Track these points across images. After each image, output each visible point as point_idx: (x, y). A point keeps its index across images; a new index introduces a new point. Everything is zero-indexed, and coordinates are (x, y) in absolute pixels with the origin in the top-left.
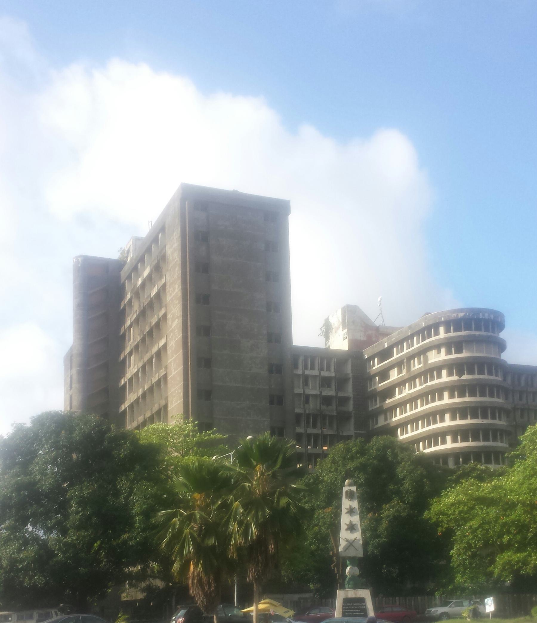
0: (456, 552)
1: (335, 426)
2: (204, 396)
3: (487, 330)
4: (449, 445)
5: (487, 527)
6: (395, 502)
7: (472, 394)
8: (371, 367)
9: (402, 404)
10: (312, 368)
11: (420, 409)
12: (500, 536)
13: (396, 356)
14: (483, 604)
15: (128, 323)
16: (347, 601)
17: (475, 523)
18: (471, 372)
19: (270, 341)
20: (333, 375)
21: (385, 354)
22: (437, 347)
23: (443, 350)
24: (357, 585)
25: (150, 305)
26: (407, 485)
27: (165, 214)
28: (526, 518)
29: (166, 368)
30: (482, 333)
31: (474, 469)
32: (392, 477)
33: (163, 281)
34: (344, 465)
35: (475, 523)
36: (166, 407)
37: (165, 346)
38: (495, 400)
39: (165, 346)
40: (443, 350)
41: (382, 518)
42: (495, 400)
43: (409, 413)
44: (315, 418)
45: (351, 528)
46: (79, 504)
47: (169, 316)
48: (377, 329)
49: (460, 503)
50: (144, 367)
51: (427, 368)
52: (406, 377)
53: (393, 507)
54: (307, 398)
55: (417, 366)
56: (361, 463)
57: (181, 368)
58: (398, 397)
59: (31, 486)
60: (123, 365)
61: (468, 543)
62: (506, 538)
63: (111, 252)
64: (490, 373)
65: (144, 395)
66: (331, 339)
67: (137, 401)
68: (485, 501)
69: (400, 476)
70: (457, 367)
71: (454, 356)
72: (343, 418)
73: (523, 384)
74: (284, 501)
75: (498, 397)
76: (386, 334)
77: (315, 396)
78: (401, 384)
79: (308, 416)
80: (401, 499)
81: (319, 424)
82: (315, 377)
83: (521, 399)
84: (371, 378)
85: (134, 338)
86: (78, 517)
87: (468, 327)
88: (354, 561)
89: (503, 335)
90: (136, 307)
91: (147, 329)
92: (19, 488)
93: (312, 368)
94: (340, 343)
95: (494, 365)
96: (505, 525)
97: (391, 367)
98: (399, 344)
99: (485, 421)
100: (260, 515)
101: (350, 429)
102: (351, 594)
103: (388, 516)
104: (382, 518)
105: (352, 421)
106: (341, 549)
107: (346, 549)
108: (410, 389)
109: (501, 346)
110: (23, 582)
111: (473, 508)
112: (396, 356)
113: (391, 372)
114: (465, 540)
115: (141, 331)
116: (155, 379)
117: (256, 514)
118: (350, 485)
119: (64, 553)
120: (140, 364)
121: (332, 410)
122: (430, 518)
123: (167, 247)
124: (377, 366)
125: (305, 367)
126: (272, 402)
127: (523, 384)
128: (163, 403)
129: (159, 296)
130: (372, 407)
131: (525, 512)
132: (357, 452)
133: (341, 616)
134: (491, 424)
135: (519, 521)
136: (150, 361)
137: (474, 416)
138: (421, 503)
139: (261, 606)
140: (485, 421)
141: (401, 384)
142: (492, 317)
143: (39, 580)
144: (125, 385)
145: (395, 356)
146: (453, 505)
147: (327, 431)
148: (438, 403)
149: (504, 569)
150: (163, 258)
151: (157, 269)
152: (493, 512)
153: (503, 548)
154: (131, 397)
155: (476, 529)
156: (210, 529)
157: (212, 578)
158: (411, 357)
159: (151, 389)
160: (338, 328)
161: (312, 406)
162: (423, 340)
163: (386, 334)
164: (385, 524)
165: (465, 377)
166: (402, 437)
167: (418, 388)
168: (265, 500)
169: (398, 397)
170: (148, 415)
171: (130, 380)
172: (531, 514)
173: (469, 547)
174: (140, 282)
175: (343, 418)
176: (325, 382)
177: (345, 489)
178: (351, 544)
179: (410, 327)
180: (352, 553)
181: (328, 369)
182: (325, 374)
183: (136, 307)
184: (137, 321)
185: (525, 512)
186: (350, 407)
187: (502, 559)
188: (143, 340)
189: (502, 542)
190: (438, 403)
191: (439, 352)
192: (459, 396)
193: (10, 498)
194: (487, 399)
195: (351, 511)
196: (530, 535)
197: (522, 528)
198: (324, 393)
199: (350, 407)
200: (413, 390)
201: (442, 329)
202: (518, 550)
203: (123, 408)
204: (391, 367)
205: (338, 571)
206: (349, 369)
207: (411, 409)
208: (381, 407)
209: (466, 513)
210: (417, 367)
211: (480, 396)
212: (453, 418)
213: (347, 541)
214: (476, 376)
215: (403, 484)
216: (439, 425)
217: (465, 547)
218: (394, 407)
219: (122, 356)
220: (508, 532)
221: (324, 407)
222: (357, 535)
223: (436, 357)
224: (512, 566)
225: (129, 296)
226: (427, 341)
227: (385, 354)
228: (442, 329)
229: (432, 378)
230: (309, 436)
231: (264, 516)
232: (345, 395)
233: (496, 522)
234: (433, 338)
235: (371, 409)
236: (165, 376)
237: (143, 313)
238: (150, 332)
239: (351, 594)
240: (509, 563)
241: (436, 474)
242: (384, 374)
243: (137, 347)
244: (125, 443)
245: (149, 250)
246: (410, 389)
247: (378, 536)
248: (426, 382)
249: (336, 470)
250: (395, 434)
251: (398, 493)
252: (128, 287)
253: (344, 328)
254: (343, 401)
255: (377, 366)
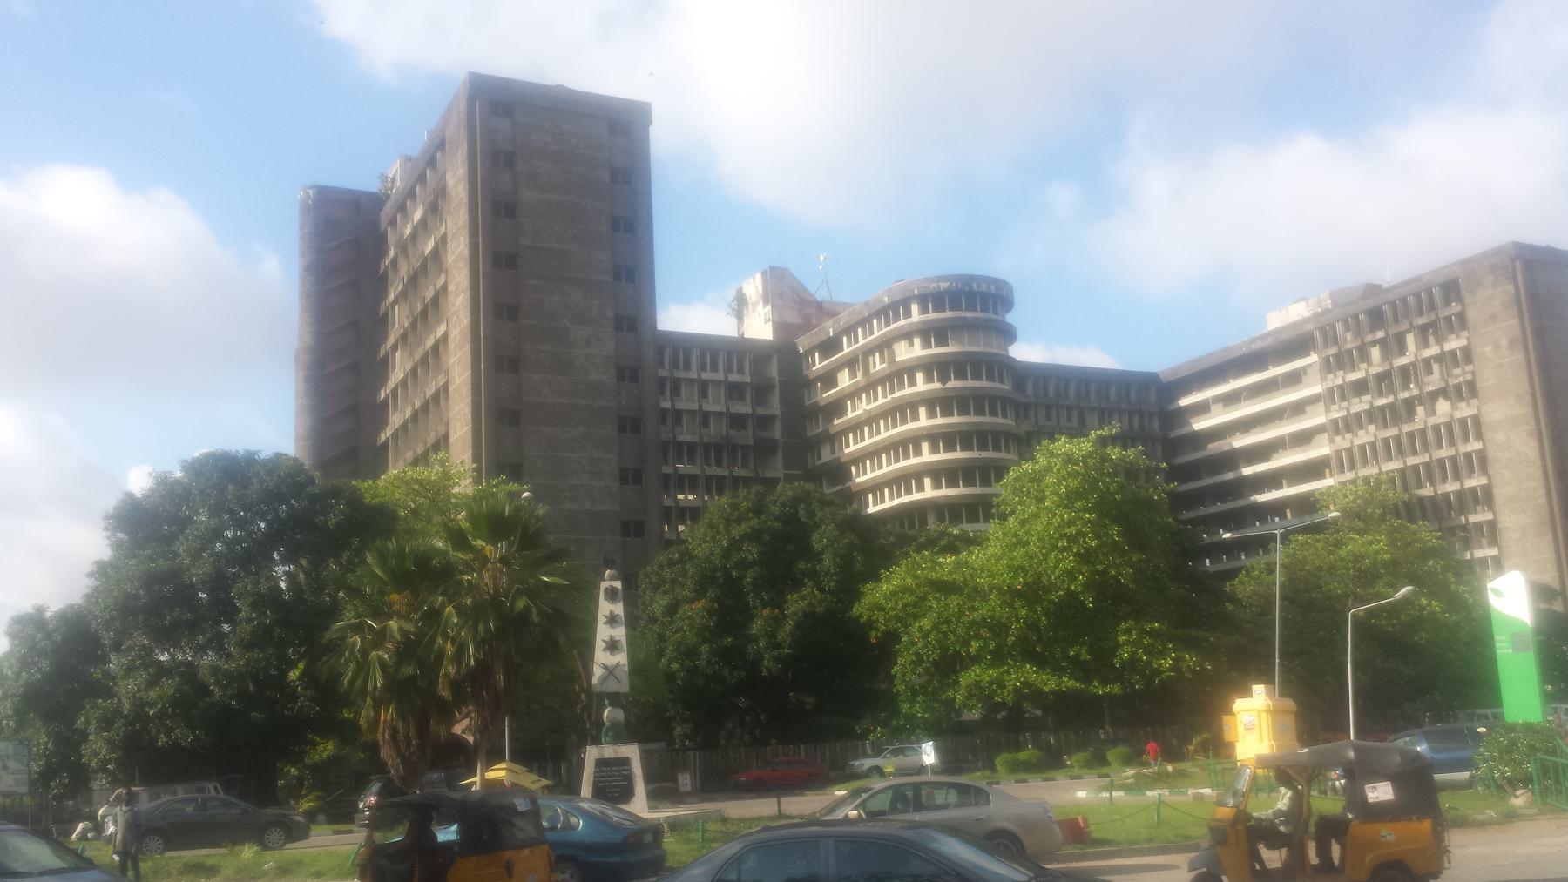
0: (903, 668)
1: (752, 466)
2: (507, 421)
3: (985, 309)
4: (929, 492)
5: (944, 628)
6: (806, 591)
7: (963, 411)
8: (809, 368)
9: (856, 427)
10: (715, 369)
11: (884, 435)
12: (967, 643)
13: (847, 349)
14: (919, 753)
15: (391, 297)
16: (602, 763)
17: (926, 623)
18: (961, 375)
19: (618, 328)
20: (748, 379)
21: (830, 346)
22: (907, 335)
23: (917, 341)
24: (623, 734)
25: (424, 266)
26: (827, 561)
27: (445, 122)
28: (1003, 613)
29: (447, 372)
30: (979, 314)
31: (943, 534)
32: (806, 551)
33: (443, 229)
34: (727, 529)
35: (926, 623)
36: (446, 437)
37: (445, 337)
38: (1000, 420)
39: (445, 337)
40: (917, 341)
41: (785, 617)
42: (1000, 420)
43: (868, 442)
44: (719, 451)
45: (612, 646)
46: (254, 606)
47: (451, 288)
48: (819, 305)
49: (905, 589)
50: (414, 371)
51: (894, 369)
52: (863, 383)
53: (803, 598)
54: (705, 417)
55: (878, 366)
56: (752, 528)
57: (468, 373)
58: (850, 415)
59: (174, 575)
60: (384, 366)
61: (917, 654)
62: (975, 645)
63: (364, 181)
64: (991, 378)
65: (415, 416)
66: (747, 321)
67: (404, 427)
68: (945, 588)
69: (817, 547)
70: (933, 367)
71: (935, 350)
72: (764, 450)
73: (1072, 394)
74: (521, 603)
75: (1005, 416)
76: (832, 314)
77: (719, 414)
78: (854, 394)
79: (707, 447)
80: (818, 584)
81: (725, 462)
82: (718, 383)
83: (1048, 418)
84: (808, 384)
85: (400, 319)
86: (249, 628)
87: (955, 306)
88: (615, 699)
89: (1011, 318)
90: (404, 270)
91: (419, 307)
92: (151, 580)
93: (715, 369)
94: (760, 327)
95: (1001, 367)
96: (973, 623)
97: (839, 367)
98: (850, 330)
99: (984, 455)
100: (481, 628)
101: (777, 469)
102: (609, 751)
103: (795, 613)
104: (785, 617)
105: (780, 455)
106: (595, 681)
107: (603, 680)
108: (869, 402)
109: (1008, 335)
110: (156, 740)
111: (924, 599)
112: (847, 349)
113: (839, 376)
114: (914, 649)
115: (412, 310)
116: (430, 392)
117: (475, 626)
118: (612, 578)
119: (224, 688)
120: (409, 366)
121: (747, 437)
122: (861, 616)
123: (449, 176)
124: (818, 364)
125: (703, 368)
126: (622, 429)
127: (1072, 394)
128: (442, 429)
129: (436, 253)
130: (813, 431)
131: (1005, 603)
132: (749, 510)
133: (1292, 742)
134: (990, 459)
135: (992, 618)
136: (424, 360)
137: (967, 446)
138: (849, 587)
139: (491, 775)
140: (984, 455)
141: (854, 394)
142: (993, 288)
143: (183, 735)
144: (387, 398)
145: (846, 350)
146: (894, 593)
147: (738, 471)
148: (910, 426)
149: (970, 696)
150: (442, 191)
151: (434, 209)
152: (954, 601)
153: (976, 660)
154: (396, 420)
155: (929, 632)
156: (408, 649)
157: (412, 729)
158: (868, 352)
159: (425, 407)
160: (757, 304)
161: (715, 431)
162: (888, 324)
163: (832, 314)
164: (789, 625)
165: (953, 384)
166: (1200, 424)
167: (881, 401)
168: (495, 604)
169: (850, 415)
170: (420, 450)
171: (394, 392)
172: (1011, 605)
173: (919, 660)
174: (408, 230)
175: (764, 450)
176: (735, 391)
177: (604, 585)
178: (610, 671)
179: (867, 304)
180: (612, 687)
181: (741, 371)
182: (734, 377)
183: (404, 270)
184: (403, 295)
185: (1005, 603)
186: (777, 432)
187: (966, 679)
188: (414, 325)
189: (968, 653)
190: (910, 426)
191: (911, 344)
192: (944, 415)
193: (136, 597)
194: (987, 419)
195: (612, 620)
196: (1011, 639)
197: (998, 628)
198: (732, 410)
199: (777, 432)
200: (874, 405)
201: (915, 308)
202: (993, 665)
203: (383, 437)
204: (839, 367)
205: (590, 716)
206: (774, 371)
207: (871, 436)
208: (826, 431)
209: (915, 605)
210: (879, 367)
211: (976, 414)
212: (934, 450)
213: (605, 667)
214: (970, 383)
215: (821, 561)
216: (913, 461)
217: (913, 662)
218: (844, 432)
219: (382, 352)
220: (978, 637)
221: (733, 433)
222: (622, 658)
223: (909, 352)
224: (982, 689)
225: (392, 253)
226: (893, 326)
227: (830, 346)
228: (915, 308)
229: (902, 386)
230: (709, 479)
231: (487, 629)
232: (768, 412)
233: (958, 620)
234: (903, 322)
235: (809, 434)
236: (446, 387)
237: (414, 281)
238: (424, 313)
239: (609, 751)
240: (977, 684)
241: (875, 544)
242: (829, 379)
243: (404, 337)
244: (337, 504)
245: (422, 178)
246: (869, 402)
247: (778, 646)
248: (892, 392)
249: (713, 538)
250: (848, 477)
251: (813, 575)
252: (391, 238)
253: (765, 304)
254: (764, 422)
255: (818, 364)
